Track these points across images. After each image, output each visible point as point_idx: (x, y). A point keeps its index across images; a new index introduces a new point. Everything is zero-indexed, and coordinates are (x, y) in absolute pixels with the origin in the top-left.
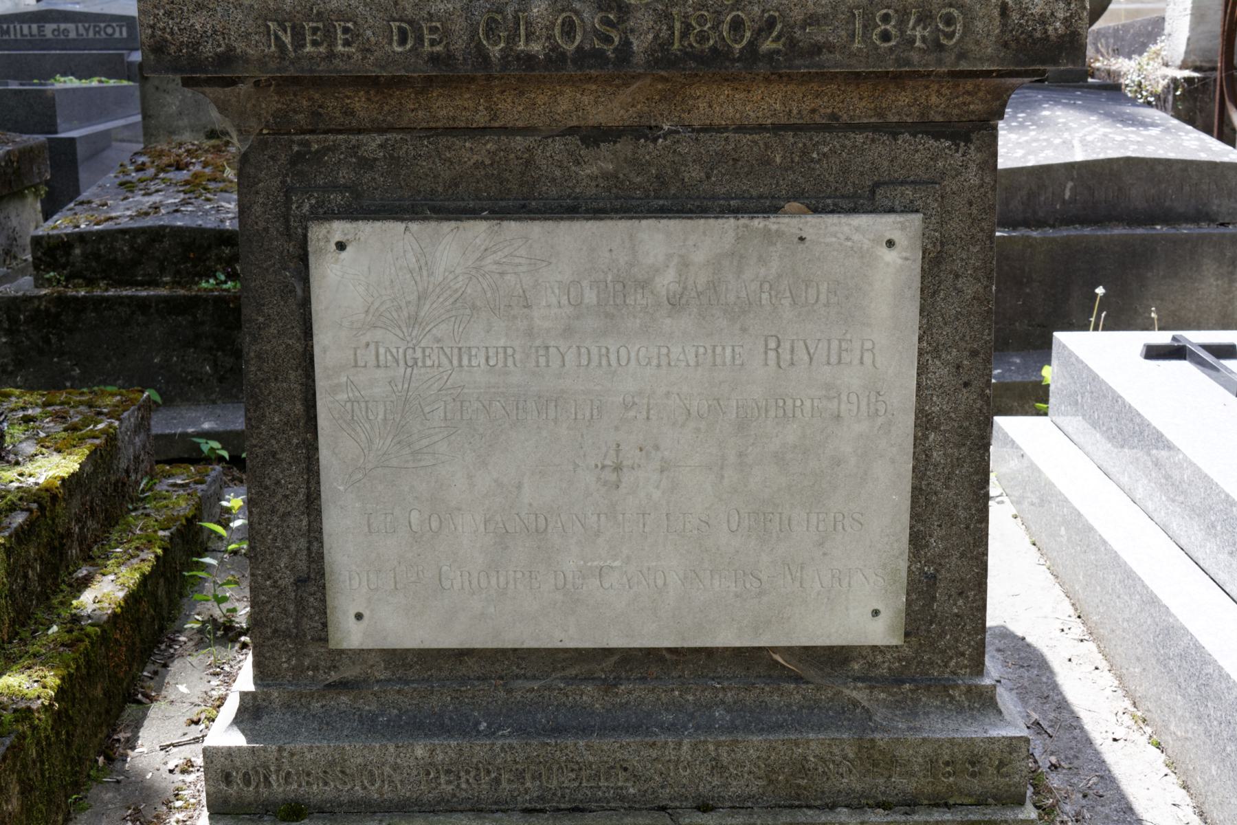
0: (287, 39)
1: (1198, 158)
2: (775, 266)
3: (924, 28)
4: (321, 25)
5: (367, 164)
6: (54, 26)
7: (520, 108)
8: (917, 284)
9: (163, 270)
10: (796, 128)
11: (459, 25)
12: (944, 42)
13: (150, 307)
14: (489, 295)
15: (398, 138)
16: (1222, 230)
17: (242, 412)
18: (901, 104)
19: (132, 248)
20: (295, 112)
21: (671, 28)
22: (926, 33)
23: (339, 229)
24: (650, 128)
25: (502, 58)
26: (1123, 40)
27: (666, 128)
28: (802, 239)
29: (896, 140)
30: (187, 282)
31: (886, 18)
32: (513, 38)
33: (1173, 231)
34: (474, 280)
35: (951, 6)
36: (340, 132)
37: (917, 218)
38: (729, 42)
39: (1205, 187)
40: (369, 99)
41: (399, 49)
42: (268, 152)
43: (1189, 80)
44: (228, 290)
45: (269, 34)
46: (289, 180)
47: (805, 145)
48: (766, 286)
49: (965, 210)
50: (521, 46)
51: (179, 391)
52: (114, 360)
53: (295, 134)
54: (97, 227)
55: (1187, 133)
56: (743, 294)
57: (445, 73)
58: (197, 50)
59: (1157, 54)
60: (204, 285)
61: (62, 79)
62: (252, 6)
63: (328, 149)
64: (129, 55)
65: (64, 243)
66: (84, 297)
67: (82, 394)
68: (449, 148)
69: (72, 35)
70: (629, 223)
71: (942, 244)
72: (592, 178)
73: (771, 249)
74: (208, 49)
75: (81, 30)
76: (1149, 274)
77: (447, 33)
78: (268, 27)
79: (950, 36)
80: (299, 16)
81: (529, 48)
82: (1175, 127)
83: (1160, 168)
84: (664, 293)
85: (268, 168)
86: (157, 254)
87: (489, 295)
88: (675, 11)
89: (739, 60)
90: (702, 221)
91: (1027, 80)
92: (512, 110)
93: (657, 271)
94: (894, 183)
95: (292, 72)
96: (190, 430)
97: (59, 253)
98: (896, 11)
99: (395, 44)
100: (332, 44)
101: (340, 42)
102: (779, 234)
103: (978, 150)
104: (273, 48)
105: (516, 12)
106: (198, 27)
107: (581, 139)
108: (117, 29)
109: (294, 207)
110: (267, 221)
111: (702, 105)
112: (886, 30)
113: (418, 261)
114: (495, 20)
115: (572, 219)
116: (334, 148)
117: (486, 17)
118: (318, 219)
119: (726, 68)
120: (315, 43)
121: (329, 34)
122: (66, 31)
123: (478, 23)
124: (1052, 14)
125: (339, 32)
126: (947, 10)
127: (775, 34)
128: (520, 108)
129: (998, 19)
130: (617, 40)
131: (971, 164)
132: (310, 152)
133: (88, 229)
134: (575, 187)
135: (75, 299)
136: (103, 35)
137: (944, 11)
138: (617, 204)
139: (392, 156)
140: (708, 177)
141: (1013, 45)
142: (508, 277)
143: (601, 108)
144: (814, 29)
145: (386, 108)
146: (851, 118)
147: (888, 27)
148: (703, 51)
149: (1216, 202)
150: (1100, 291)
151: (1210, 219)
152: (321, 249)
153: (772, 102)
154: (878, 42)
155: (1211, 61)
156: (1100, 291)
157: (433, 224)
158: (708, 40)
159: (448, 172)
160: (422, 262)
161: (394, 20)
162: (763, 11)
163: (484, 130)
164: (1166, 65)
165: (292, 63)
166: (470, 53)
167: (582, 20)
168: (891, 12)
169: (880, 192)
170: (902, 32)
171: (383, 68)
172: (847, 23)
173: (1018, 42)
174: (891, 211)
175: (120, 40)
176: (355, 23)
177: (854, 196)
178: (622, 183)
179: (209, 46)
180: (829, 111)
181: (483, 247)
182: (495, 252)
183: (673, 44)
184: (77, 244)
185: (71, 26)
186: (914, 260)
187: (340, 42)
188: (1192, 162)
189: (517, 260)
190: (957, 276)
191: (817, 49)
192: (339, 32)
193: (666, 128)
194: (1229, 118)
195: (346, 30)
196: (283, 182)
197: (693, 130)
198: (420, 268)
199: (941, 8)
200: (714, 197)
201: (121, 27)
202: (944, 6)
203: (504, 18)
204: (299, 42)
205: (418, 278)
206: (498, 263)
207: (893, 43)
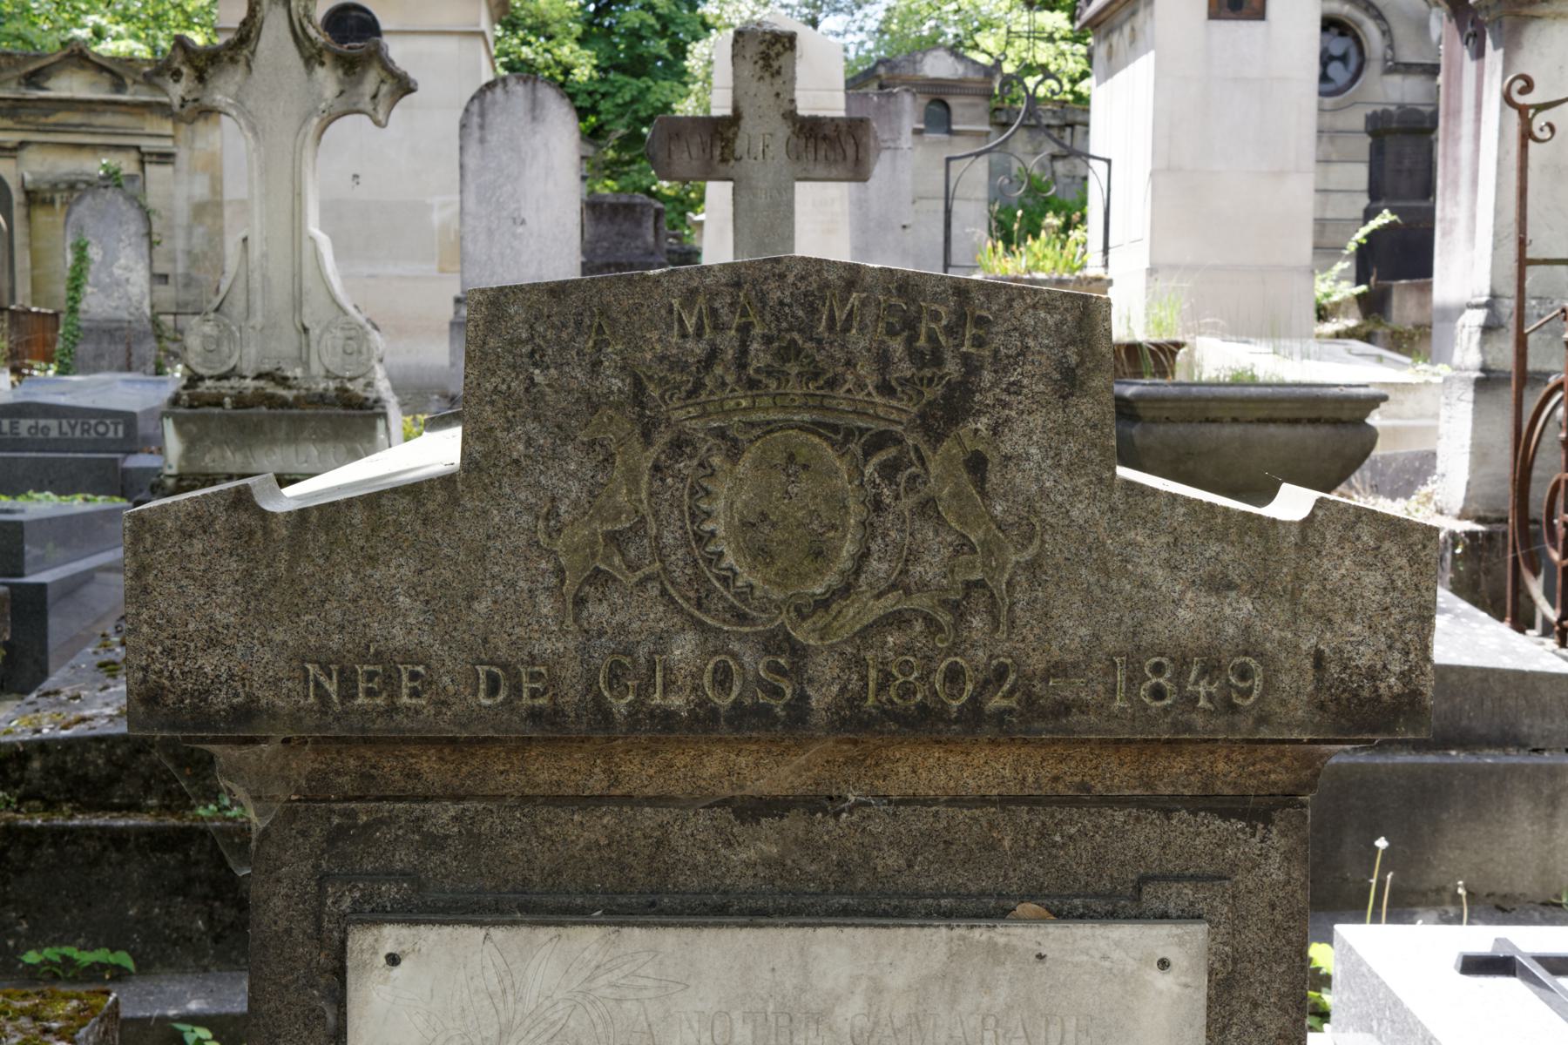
0: (332, 687)
1: (1501, 666)
2: (1003, 994)
3: (1211, 683)
4: (379, 669)
5: (435, 843)
6: (31, 422)
7: (651, 772)
8: (1201, 1019)
9: (148, 790)
10: (1032, 802)
11: (571, 671)
12: (1238, 700)
13: (128, 840)
14: (600, 1029)
15: (480, 807)
16: (1535, 759)
17: (245, 984)
18: (1175, 774)
19: (109, 761)
20: (338, 773)
21: (864, 678)
22: (1213, 689)
23: (391, 936)
24: (831, 798)
25: (630, 715)
26: (1382, 474)
27: (852, 799)
28: (1040, 957)
29: (1169, 819)
30: (179, 807)
31: (1158, 669)
32: (645, 688)
33: (1473, 760)
34: (580, 1009)
35: (1246, 653)
36: (399, 799)
37: (1199, 931)
38: (942, 696)
39: (1511, 703)
40: (441, 759)
41: (487, 702)
42: (297, 826)
43: (1471, 535)
44: (233, 820)
45: (306, 680)
46: (324, 864)
47: (1044, 824)
48: (991, 1021)
49: (1265, 915)
50: (657, 699)
51: (160, 952)
52: (75, 911)
53: (337, 801)
54: (64, 733)
55: (1482, 623)
56: (958, 1033)
57: (550, 728)
58: (205, 700)
59: (1429, 498)
60: (201, 811)
61: (37, 496)
62: (285, 643)
63: (381, 821)
64: (124, 460)
65: (17, 753)
66: (40, 827)
67: (25, 996)
68: (550, 822)
69: (54, 434)
70: (799, 932)
71: (1235, 961)
72: (747, 864)
73: (998, 970)
74: (220, 700)
75: (66, 428)
76: (1445, 816)
77: (554, 681)
78: (307, 671)
79: (1246, 693)
80: (350, 656)
81: (667, 702)
82: (1465, 614)
83: (1454, 677)
84: (847, 1029)
85: (296, 847)
86: (142, 769)
87: (600, 1029)
88: (869, 655)
89: (957, 721)
90: (902, 931)
91: (1348, 747)
92: (639, 773)
93: (838, 998)
94: (1166, 878)
95: (336, 730)
96: (171, 1012)
97: (11, 766)
98: (1172, 660)
99: (481, 695)
100: (394, 694)
101: (405, 691)
102: (1009, 949)
103: (1283, 834)
104: (312, 699)
105: (651, 654)
106: (208, 669)
107: (734, 812)
108: (112, 428)
109: (329, 902)
110: (290, 919)
111: (903, 769)
112: (1158, 684)
113: (501, 981)
114: (620, 665)
115: (720, 925)
116: (390, 821)
117: (609, 660)
118: (362, 922)
119: (939, 732)
120: (370, 693)
121: (390, 681)
122: (47, 429)
123: (598, 669)
124: (1385, 667)
125: (405, 677)
126: (1242, 659)
127: (1006, 687)
128: (651, 772)
129: (1311, 672)
130: (788, 692)
131: (1273, 853)
132: (355, 826)
133: (52, 735)
134: (724, 875)
135: (29, 829)
136: (93, 434)
137: (1237, 661)
138: (783, 902)
139: (469, 832)
140: (910, 866)
141: (1332, 707)
142: (627, 1005)
143: (763, 771)
144: (1061, 682)
145: (465, 769)
146: (1108, 789)
147: (1161, 680)
148: (907, 709)
149: (1527, 721)
150: (1381, 843)
151: (1520, 743)
152: (365, 965)
153: (999, 767)
154: (1147, 700)
155: (1496, 511)
156: (1381, 843)
157: (525, 931)
158: (915, 694)
159: (548, 854)
160: (507, 983)
161: (482, 663)
162: (991, 657)
163: (600, 800)
164: (1441, 512)
165: (337, 719)
166: (585, 708)
167: (742, 666)
168: (1165, 660)
169: (1148, 889)
170: (1181, 688)
171: (463, 726)
172: (1106, 674)
173: (1339, 704)
174: (1163, 917)
175: (114, 441)
176: (428, 667)
177: (1110, 896)
178: (790, 872)
179: (222, 695)
180: (1077, 779)
181: (593, 964)
182: (610, 970)
183: (866, 699)
184: (36, 755)
185: (53, 423)
186: (1197, 988)
187: (405, 691)
188: (1493, 671)
189: (641, 982)
190: (1255, 1005)
191: (1064, 708)
192: (405, 677)
193: (852, 799)
194: (1526, 587)
195: (414, 676)
196: (316, 867)
197: (890, 802)
198: (504, 991)
199: (1233, 657)
200: (918, 895)
201: (116, 425)
202: (1237, 654)
203: (634, 661)
204: (348, 693)
205: (501, 1006)
206: (612, 985)
207: (1168, 701)
